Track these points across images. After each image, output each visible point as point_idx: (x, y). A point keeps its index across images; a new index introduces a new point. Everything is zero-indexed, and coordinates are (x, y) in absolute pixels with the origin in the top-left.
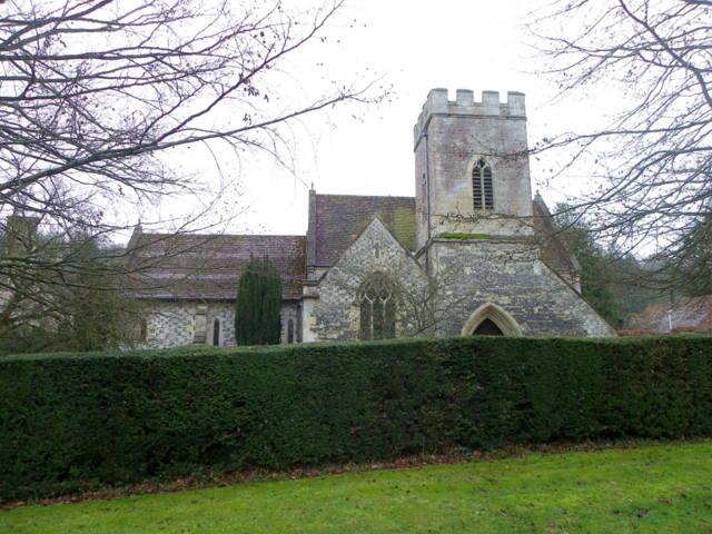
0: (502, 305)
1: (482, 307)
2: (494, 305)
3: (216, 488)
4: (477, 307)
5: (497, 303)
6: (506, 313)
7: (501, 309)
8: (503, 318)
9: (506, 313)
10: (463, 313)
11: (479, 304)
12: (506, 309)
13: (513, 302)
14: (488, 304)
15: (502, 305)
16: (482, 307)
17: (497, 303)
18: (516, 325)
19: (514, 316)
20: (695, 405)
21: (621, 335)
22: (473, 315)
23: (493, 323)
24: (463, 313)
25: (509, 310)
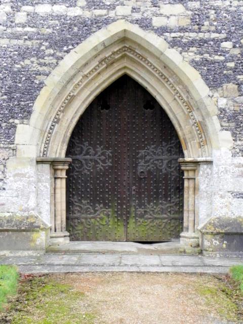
0: (161, 31)
1: (99, 37)
2: (135, 29)
3: (223, 272)
4: (78, 39)
5: (145, 24)
6: (173, 55)
7: (156, 42)
8: (167, 72)
9: (173, 55)
10: (39, 54)
11: (87, 27)
12: (174, 43)
13: (197, 20)
14: (115, 29)
15: (161, 31)
16: (99, 37)
17: (145, 24)
18: (200, 88)
19: (196, 65)
20: (236, 296)
21: (193, 138)
22: (70, 60)
23: (150, 102)
24: (39, 54)
25: (184, 46)
